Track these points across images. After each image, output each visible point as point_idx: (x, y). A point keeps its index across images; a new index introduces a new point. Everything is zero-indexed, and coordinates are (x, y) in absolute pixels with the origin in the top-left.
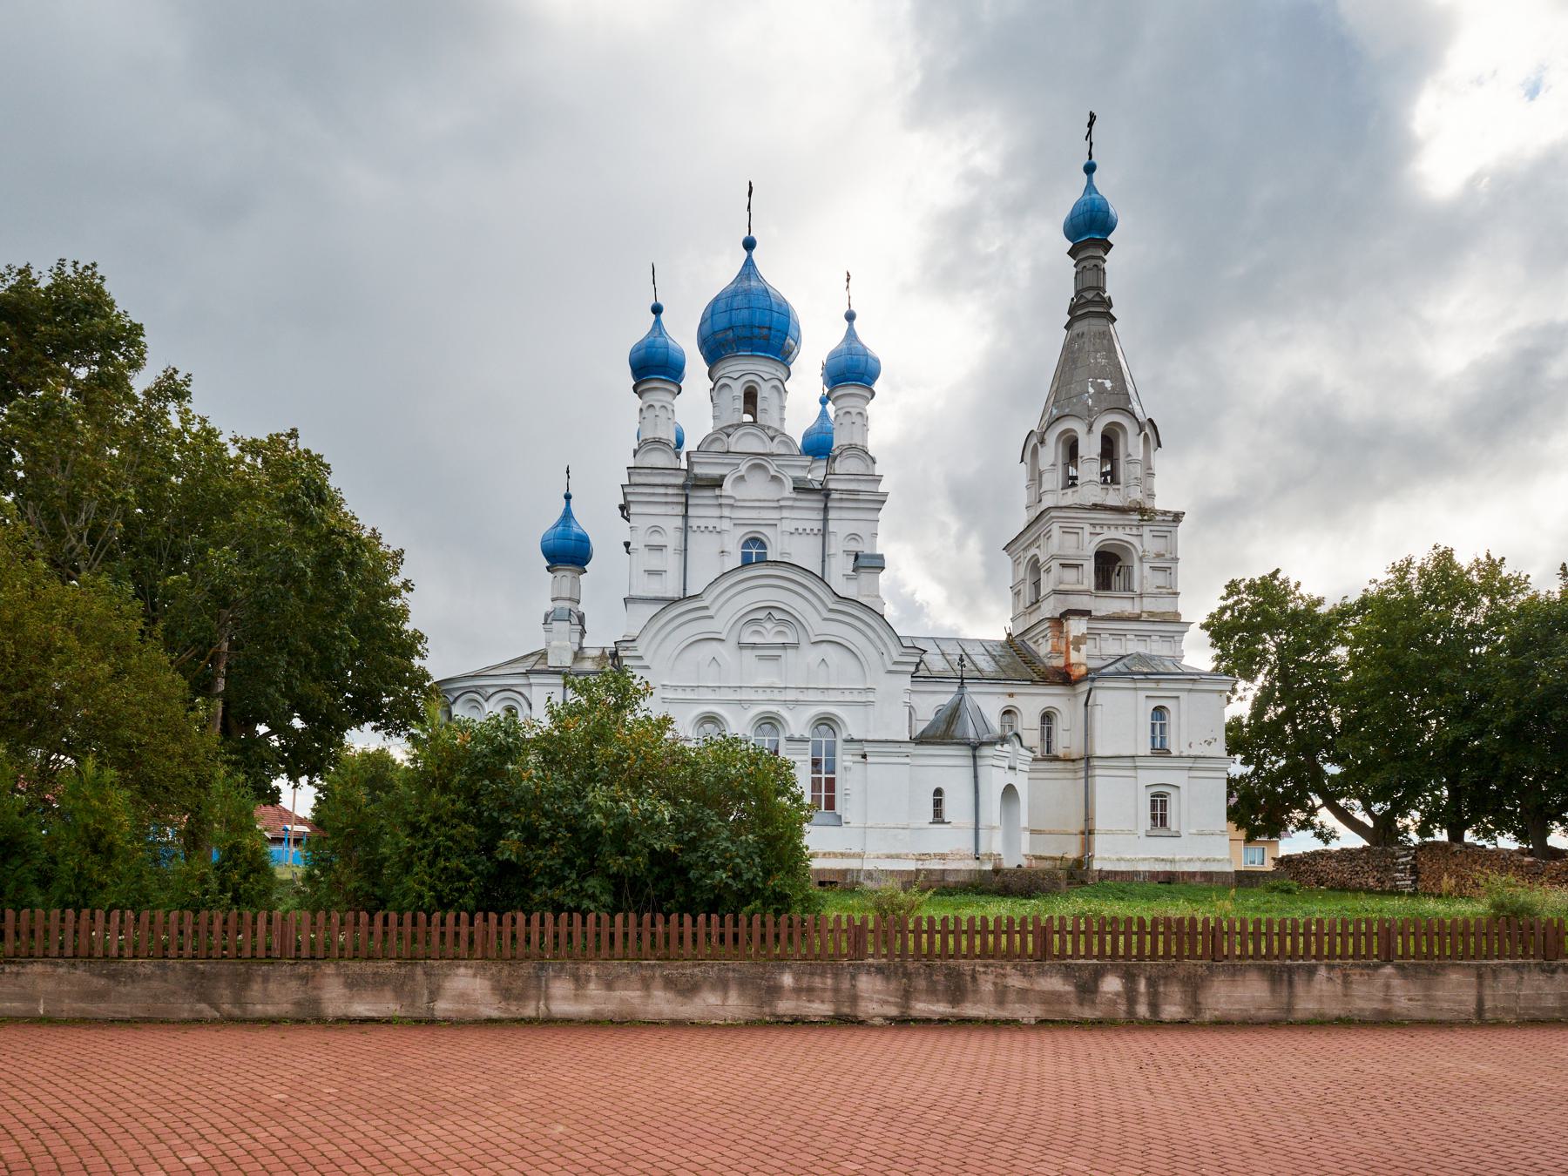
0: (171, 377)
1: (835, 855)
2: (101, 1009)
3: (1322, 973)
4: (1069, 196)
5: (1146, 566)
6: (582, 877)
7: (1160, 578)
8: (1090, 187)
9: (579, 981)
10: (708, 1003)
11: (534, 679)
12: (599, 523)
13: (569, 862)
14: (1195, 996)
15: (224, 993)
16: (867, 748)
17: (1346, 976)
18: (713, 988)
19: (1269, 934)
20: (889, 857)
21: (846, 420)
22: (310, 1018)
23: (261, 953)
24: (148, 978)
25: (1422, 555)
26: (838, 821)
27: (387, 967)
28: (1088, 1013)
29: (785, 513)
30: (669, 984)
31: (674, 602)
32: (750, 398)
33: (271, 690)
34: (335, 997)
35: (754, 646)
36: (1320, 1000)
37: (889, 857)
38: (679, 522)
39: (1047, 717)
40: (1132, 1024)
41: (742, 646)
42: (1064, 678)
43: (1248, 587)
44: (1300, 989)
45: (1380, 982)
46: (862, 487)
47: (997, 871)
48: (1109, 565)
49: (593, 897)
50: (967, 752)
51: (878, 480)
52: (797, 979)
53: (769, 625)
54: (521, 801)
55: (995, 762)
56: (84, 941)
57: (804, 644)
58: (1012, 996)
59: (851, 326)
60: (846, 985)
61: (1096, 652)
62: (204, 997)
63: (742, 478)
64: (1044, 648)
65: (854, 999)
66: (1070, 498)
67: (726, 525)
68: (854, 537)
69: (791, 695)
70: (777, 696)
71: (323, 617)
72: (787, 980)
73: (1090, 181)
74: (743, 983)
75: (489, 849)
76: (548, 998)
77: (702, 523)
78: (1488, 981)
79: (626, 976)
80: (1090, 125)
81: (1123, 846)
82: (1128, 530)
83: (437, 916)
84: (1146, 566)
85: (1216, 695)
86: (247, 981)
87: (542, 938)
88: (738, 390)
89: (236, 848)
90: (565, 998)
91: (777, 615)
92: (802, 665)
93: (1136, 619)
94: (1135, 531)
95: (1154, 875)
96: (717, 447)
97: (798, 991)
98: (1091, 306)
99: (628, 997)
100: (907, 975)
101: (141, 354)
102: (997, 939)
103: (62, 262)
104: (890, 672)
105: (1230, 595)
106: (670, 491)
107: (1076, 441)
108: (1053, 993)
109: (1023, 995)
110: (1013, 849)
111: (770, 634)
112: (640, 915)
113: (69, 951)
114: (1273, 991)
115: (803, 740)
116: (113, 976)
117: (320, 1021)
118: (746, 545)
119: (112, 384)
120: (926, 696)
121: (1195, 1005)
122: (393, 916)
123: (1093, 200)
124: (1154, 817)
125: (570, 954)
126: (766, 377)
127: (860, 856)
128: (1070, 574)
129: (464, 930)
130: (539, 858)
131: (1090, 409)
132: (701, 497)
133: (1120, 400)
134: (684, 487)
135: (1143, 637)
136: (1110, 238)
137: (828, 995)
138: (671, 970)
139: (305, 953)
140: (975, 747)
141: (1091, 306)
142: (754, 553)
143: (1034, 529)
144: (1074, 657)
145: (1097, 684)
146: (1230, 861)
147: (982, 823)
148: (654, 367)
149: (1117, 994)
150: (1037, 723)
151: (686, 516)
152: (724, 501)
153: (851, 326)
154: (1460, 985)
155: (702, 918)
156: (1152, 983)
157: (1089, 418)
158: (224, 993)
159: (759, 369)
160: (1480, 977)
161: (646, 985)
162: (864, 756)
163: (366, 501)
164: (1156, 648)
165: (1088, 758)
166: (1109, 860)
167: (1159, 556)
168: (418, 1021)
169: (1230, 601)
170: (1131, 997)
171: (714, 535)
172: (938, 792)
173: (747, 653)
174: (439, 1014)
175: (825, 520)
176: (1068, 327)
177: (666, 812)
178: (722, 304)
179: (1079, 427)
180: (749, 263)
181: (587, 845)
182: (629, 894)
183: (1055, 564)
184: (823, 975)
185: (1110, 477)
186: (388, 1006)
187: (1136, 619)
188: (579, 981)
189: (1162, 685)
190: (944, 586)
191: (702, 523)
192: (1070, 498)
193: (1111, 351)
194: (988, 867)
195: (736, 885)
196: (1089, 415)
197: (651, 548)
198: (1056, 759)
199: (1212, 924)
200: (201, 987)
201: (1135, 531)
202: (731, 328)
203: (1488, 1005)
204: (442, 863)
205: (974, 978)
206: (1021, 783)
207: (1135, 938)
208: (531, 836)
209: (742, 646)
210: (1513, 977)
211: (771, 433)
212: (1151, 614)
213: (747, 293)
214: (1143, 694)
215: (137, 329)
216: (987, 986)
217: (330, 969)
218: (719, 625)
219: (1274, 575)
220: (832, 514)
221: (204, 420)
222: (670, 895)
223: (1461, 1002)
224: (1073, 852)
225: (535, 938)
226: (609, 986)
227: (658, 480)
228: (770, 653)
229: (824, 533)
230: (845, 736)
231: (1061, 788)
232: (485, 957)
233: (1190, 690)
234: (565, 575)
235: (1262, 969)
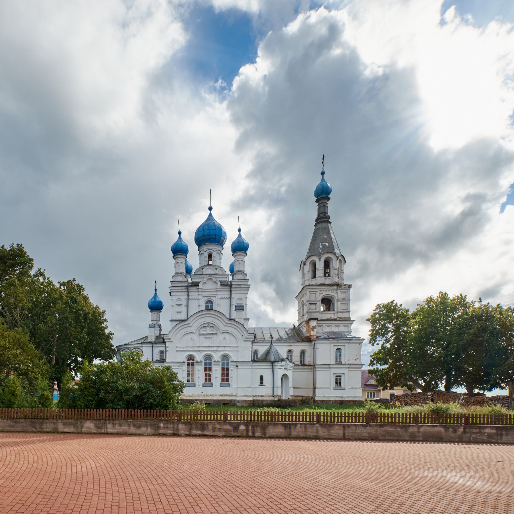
0: (40, 270)
1: (228, 395)
2: (13, 429)
3: (299, 425)
4: (316, 182)
5: (339, 303)
6: (119, 401)
7: (344, 306)
8: (323, 179)
9: (114, 425)
10: (143, 430)
11: (144, 345)
12: (164, 297)
13: (116, 397)
14: (264, 431)
15: (38, 426)
16: (238, 364)
17: (305, 427)
18: (144, 427)
20: (245, 396)
21: (238, 263)
22: (55, 432)
23: (45, 418)
24: (22, 423)
25: (435, 296)
26: (229, 385)
27: (72, 421)
28: (236, 434)
29: (218, 293)
30: (134, 425)
31: (184, 321)
32: (210, 256)
33: (65, 353)
34: (61, 427)
35: (204, 334)
36: (298, 432)
37: (245, 396)
38: (186, 297)
39: (303, 353)
40: (247, 437)
41: (200, 335)
42: (309, 340)
43: (383, 306)
44: (292, 429)
45: (315, 428)
46: (243, 283)
47: (279, 400)
48: (327, 302)
49: (120, 406)
50: (270, 364)
51: (247, 281)
52: (164, 425)
53: (208, 328)
54: (104, 384)
55: (279, 367)
56: (9, 415)
57: (219, 333)
58: (217, 430)
59: (240, 233)
60: (176, 426)
61: (321, 331)
62: (34, 427)
63: (205, 283)
64: (304, 330)
65: (178, 430)
66: (314, 282)
67: (200, 297)
68: (240, 299)
69: (214, 349)
70: (211, 349)
71: (78, 332)
72: (162, 425)
73: (323, 177)
74: (151, 426)
75: (97, 395)
76: (107, 428)
77: (193, 297)
78: (347, 428)
79: (124, 424)
80: (323, 159)
81: (326, 391)
82: (333, 291)
83: (86, 410)
84: (339, 303)
85: (358, 344)
86: (42, 424)
88: (206, 255)
89: (43, 395)
90: (111, 428)
91: (211, 325)
92: (218, 340)
93: (335, 320)
95: (335, 402)
96: (199, 273)
97: (164, 428)
98: (323, 219)
99: (125, 428)
100: (191, 424)
101: (32, 266)
103: (13, 244)
105: (377, 309)
106: (183, 288)
108: (227, 429)
109: (220, 430)
110: (289, 393)
111: (208, 331)
112: (134, 410)
113: (6, 417)
114: (285, 430)
115: (218, 362)
116: (15, 422)
117: (58, 432)
118: (207, 303)
119: (24, 274)
120: (263, 347)
121: (264, 433)
122: (80, 410)
123: (323, 184)
124: (336, 383)
125: (112, 418)
126: (215, 250)
127: (235, 396)
128: (313, 307)
129: (89, 413)
130: (109, 397)
131: (320, 253)
133: (331, 250)
134: (187, 286)
135: (337, 326)
136: (330, 196)
137: (172, 429)
138: (135, 422)
139: (55, 418)
140: (273, 363)
142: (209, 305)
143: (302, 292)
144: (312, 333)
145: (317, 342)
146: (362, 397)
147: (275, 386)
148: (179, 250)
149: (244, 430)
150: (299, 354)
151: (188, 295)
152: (199, 290)
153: (240, 233)
154: (338, 429)
155: (149, 410)
156: (253, 427)
157: (319, 256)
158: (38, 426)
159: (212, 248)
160: (344, 427)
161: (129, 426)
162: (237, 366)
163: (95, 297)
164: (341, 329)
165: (314, 365)
166: (321, 397)
167: (343, 299)
168: (78, 433)
169: (377, 311)
170: (247, 430)
171: (197, 300)
172: (261, 376)
173: (202, 337)
174: (83, 432)
175: (231, 294)
176: (315, 225)
177: (136, 386)
178: (201, 229)
179: (316, 259)
180: (210, 215)
181: (120, 393)
182: (129, 405)
183: (307, 303)
184: (170, 424)
185: (326, 274)
186: (72, 430)
187: (335, 320)
188: (114, 425)
190: (275, 312)
191: (193, 297)
192: (314, 282)
193: (329, 233)
194: (276, 399)
195: (155, 403)
196: (322, 255)
197: (178, 305)
198: (306, 365)
200: (33, 425)
201: (335, 292)
202: (204, 236)
203: (347, 434)
204: (87, 398)
205: (207, 425)
206: (290, 373)
208: (107, 392)
209: (200, 335)
210: (354, 428)
211: (216, 267)
212: (340, 318)
213: (208, 225)
215: (31, 260)
216: (210, 427)
217: (60, 421)
218: (193, 329)
219: (392, 302)
220: (233, 292)
221: (48, 278)
222: (141, 405)
223: (338, 434)
224: (311, 395)
225: (104, 415)
226: (121, 426)
227: (179, 285)
229: (230, 298)
230: (231, 360)
231: (305, 374)
232: (93, 419)
233: (349, 343)
234: (155, 313)
235: (282, 424)
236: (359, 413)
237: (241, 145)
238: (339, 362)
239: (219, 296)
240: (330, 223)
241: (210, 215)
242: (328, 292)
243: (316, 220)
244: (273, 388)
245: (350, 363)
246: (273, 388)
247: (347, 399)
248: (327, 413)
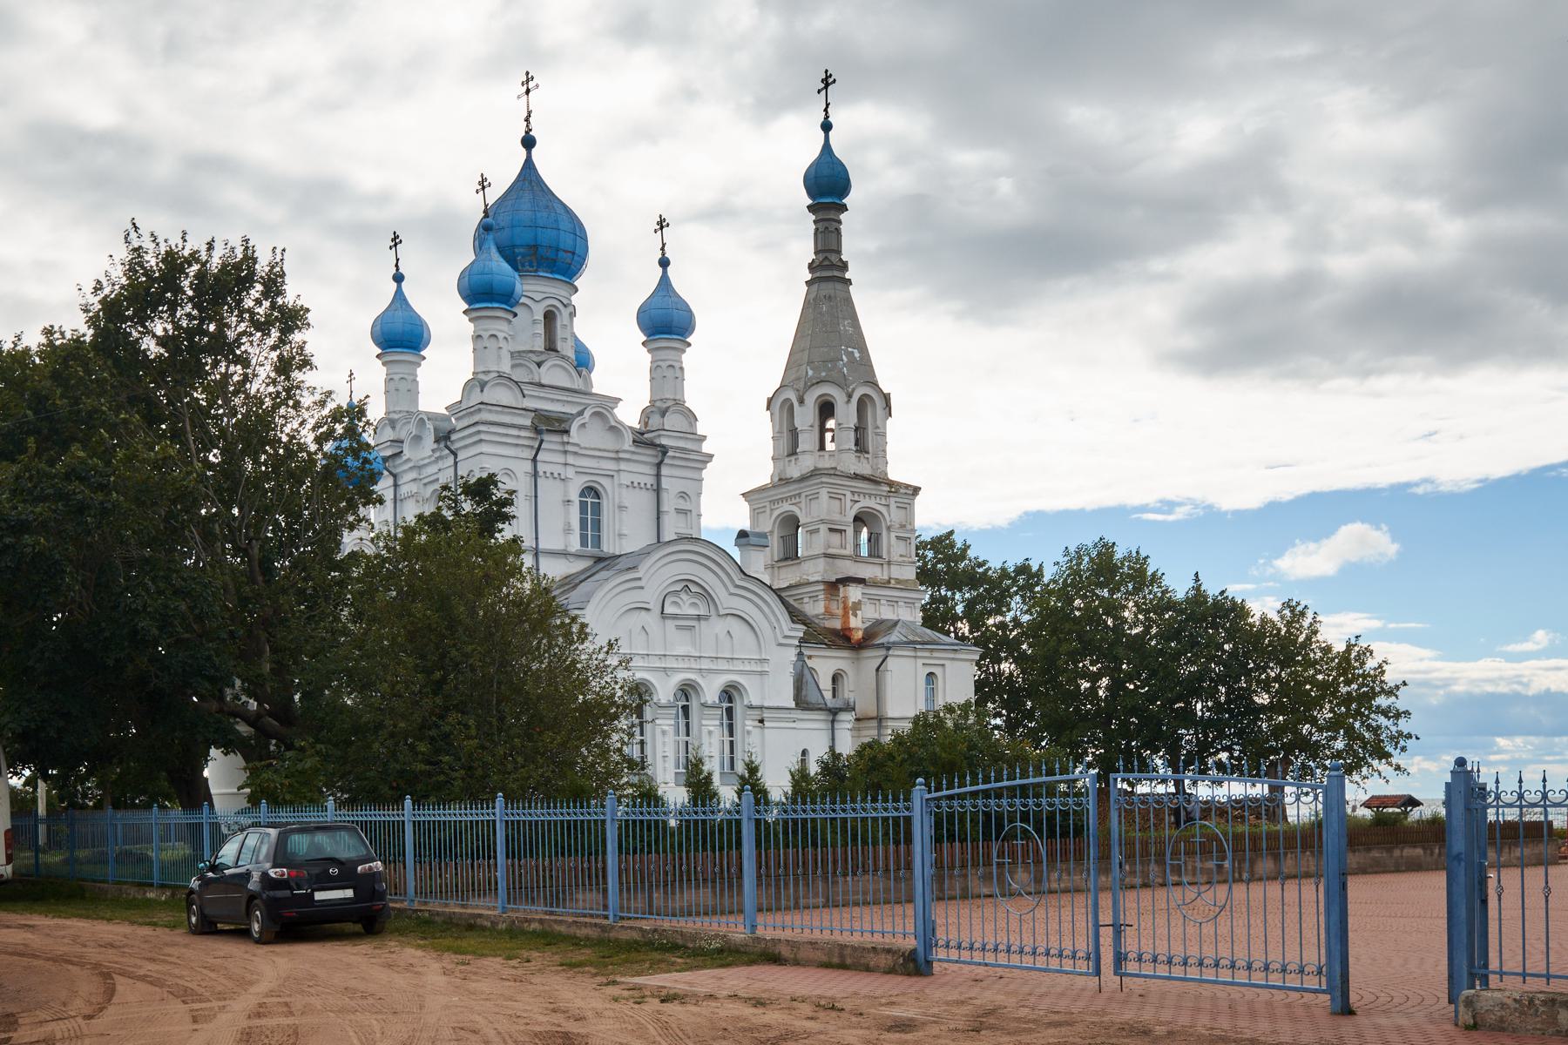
29: (623, 466)
38: (528, 466)
39: (835, 679)
53: (684, 596)
67: (570, 472)
69: (705, 665)
91: (694, 588)
93: (885, 584)
104: (780, 645)
118: (582, 494)
126: (538, 297)
128: (836, 538)
141: (828, 270)
152: (570, 448)
162: (761, 721)
167: (903, 526)
173: (670, 624)
175: (658, 476)
179: (838, 396)
183: (823, 528)
185: (861, 446)
187: (885, 584)
189: (935, 654)
212: (898, 581)
214: (920, 662)
220: (665, 471)
228: (689, 624)
229: (658, 490)
240: (849, 282)
241: (529, 165)
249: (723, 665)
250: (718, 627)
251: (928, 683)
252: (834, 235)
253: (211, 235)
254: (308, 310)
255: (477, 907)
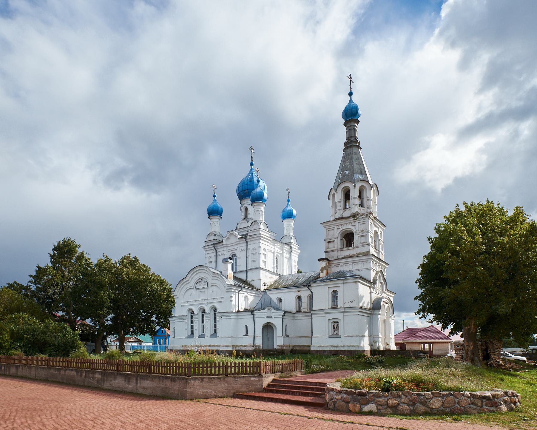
4: (343, 103)
19: (215, 367)
20: (226, 346)
29: (239, 246)
37: (226, 346)
38: (215, 254)
53: (202, 283)
63: (228, 238)
69: (206, 302)
82: (350, 225)
87: (8, 359)
94: (353, 224)
95: (331, 352)
102: (242, 369)
107: (349, 191)
132: (219, 247)
175: (247, 245)
178: (241, 185)
187: (353, 256)
189: (333, 283)
199: (225, 364)
207: (209, 369)
212: (359, 254)
214: (327, 287)
228: (202, 290)
229: (247, 250)
236: (231, 363)
237: (464, 64)
238: (335, 306)
239: (239, 249)
242: (347, 226)
243: (345, 144)
244: (254, 337)
245: (345, 306)
246: (254, 337)
247: (342, 349)
248: (235, 363)
249: (210, 301)
250: (211, 289)
251: (334, 294)
252: (353, 131)
253: (58, 238)
254: (445, 217)
255: (386, 337)
